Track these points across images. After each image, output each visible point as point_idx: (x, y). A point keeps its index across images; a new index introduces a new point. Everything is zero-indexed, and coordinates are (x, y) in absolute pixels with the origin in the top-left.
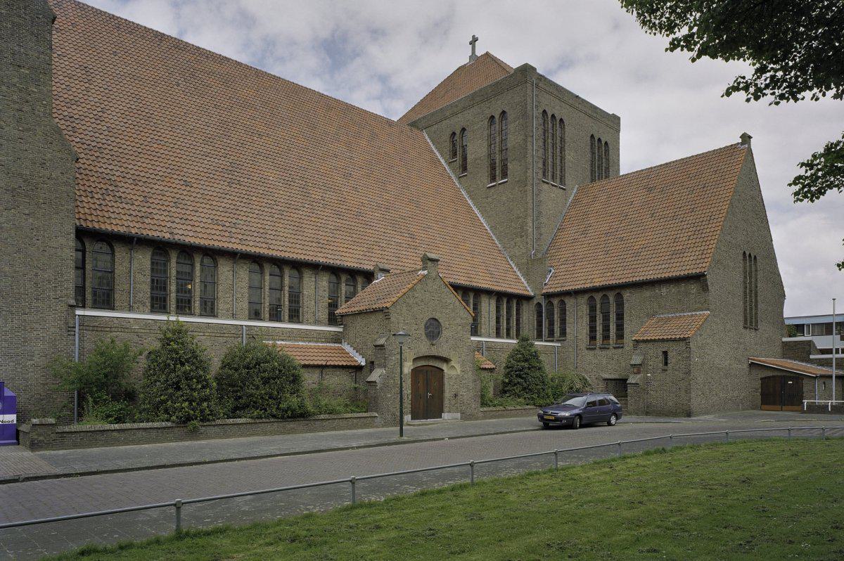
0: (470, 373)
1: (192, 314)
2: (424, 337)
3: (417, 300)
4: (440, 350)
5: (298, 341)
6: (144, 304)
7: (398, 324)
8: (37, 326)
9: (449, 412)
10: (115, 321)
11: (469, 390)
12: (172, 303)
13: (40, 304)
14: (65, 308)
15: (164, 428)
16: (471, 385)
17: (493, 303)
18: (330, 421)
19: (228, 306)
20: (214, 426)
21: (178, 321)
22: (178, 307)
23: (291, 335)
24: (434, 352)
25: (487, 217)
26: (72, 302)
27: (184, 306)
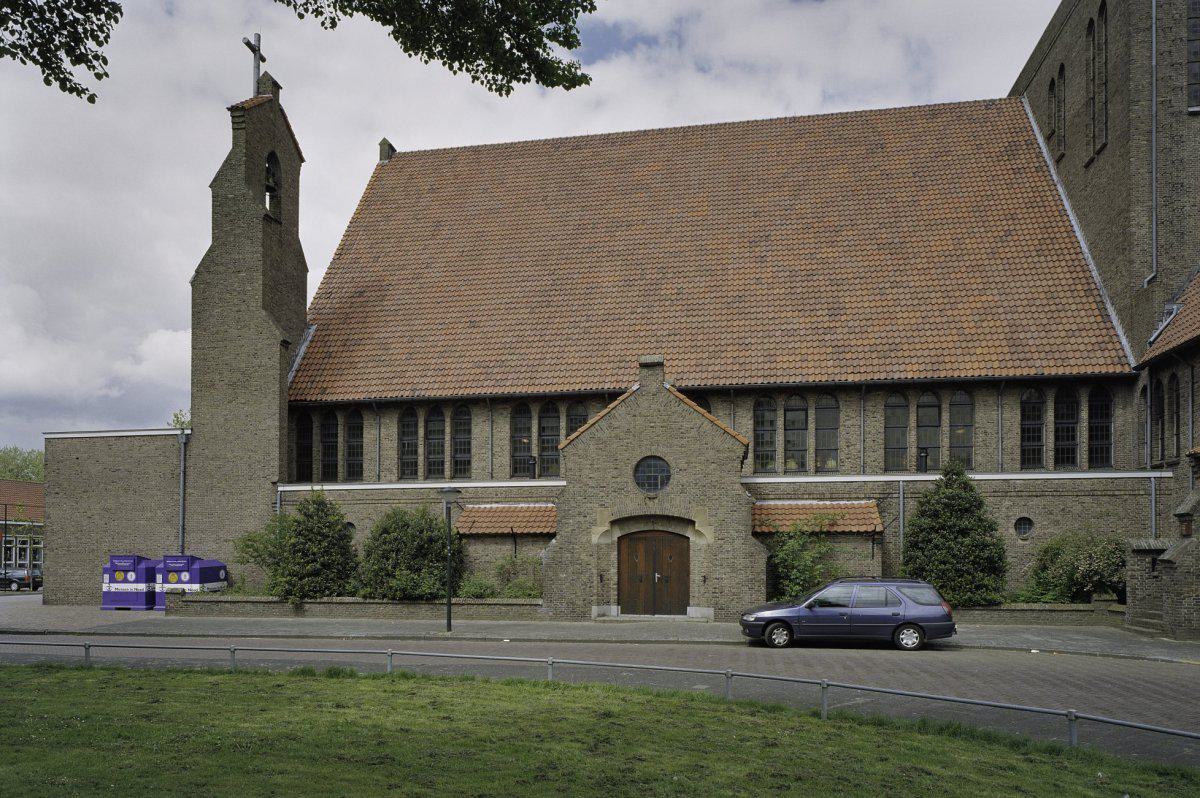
0: (738, 543)
1: (774, 472)
2: (632, 485)
3: (617, 431)
4: (667, 505)
5: (519, 502)
6: (391, 472)
7: (581, 470)
8: (250, 504)
9: (698, 605)
10: (782, 488)
11: (734, 570)
12: (1049, 454)
13: (252, 483)
14: (269, 485)
15: (270, 602)
16: (741, 562)
17: (503, 428)
18: (466, 607)
19: (484, 464)
20: (320, 603)
21: (313, 491)
22: (1091, 460)
23: (796, 493)
24: (654, 508)
25: (1085, 226)
26: (276, 479)
27: (330, 476)
